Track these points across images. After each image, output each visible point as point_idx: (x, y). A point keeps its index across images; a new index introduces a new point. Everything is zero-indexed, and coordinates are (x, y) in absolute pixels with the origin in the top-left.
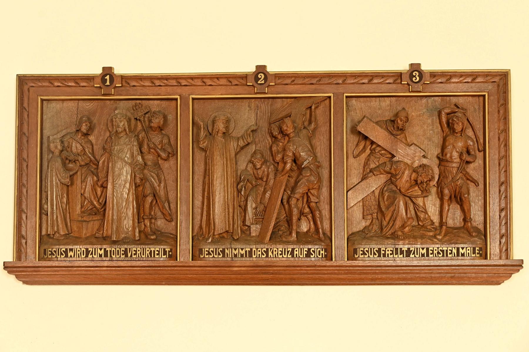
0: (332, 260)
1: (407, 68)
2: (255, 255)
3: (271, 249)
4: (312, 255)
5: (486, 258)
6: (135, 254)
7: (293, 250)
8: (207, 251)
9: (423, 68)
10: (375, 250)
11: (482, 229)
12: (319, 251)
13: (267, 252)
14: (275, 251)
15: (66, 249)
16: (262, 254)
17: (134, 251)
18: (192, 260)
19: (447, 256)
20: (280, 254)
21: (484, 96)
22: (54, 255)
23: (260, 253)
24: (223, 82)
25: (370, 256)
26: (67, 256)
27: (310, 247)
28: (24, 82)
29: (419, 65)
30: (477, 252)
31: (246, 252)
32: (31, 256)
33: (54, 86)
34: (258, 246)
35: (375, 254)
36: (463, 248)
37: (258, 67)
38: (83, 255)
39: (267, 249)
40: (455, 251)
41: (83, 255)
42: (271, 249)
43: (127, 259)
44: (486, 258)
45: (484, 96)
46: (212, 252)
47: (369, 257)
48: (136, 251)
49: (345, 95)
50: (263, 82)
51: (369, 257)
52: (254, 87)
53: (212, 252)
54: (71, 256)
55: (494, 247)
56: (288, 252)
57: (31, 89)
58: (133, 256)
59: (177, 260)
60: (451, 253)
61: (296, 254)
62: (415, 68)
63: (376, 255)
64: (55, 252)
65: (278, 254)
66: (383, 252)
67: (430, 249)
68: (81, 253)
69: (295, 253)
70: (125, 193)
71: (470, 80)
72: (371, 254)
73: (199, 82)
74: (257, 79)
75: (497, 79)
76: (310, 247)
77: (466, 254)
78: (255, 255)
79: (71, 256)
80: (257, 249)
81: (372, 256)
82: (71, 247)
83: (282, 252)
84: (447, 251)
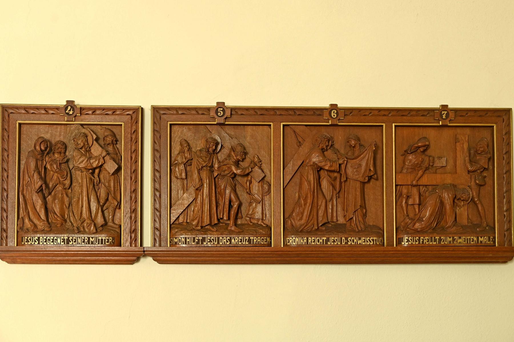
0: (121, 246)
1: (215, 104)
5: (120, 245)
7: (39, 238)
9: (76, 103)
13: (230, 240)
18: (17, 245)
19: (105, 243)
21: (171, 125)
23: (225, 241)
24: (414, 113)
28: (508, 111)
29: (224, 103)
30: (491, 240)
31: (323, 240)
33: (238, 115)
34: (223, 236)
36: (481, 237)
37: (218, 103)
40: (183, 240)
43: (198, 245)
44: (120, 245)
45: (171, 125)
49: (169, 123)
50: (443, 112)
52: (76, 116)
55: (125, 237)
56: (246, 240)
60: (108, 242)
62: (70, 103)
64: (30, 239)
66: (421, 240)
73: (252, 112)
74: (217, 112)
75: (130, 112)
77: (100, 242)
84: (105, 240)
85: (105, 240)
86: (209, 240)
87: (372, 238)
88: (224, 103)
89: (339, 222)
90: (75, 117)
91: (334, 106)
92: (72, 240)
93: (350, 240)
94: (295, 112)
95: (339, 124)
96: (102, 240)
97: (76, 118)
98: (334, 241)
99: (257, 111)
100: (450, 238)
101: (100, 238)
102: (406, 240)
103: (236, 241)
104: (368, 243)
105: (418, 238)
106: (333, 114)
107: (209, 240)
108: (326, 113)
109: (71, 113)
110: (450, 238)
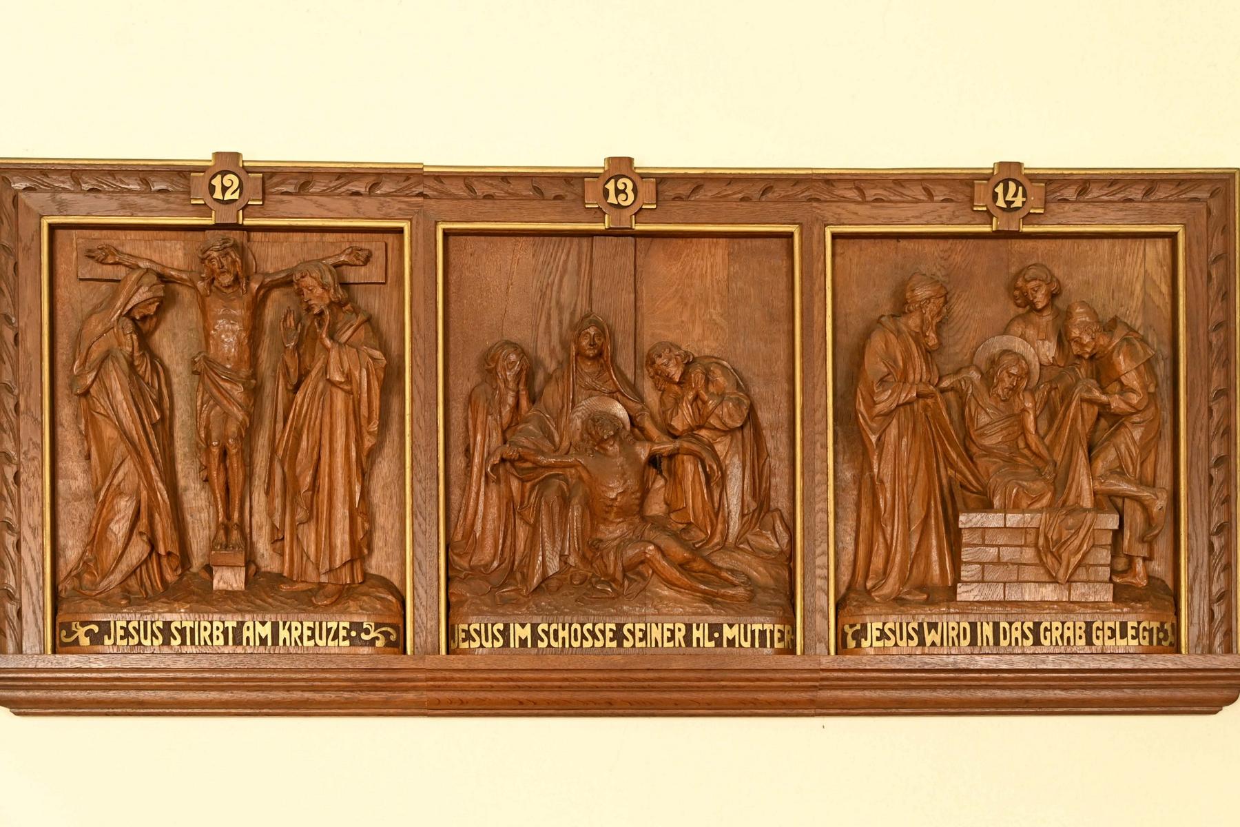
0: (1178, 651)
2: (1005, 638)
3: (285, 623)
4: (542, 640)
6: (669, 640)
8: (122, 628)
10: (910, 627)
11: (1170, 583)
12: (556, 632)
14: (205, 629)
15: (920, 625)
16: (1024, 636)
17: (309, 628)
18: (448, 652)
20: (310, 638)
22: (889, 639)
23: (1018, 634)
25: (899, 643)
26: (922, 643)
27: (168, 617)
29: (630, 160)
32: (29, 643)
35: (910, 637)
37: (612, 161)
38: (965, 638)
39: (920, 625)
41: (965, 638)
42: (285, 623)
45: (53, 228)
46: (478, 632)
47: (896, 645)
48: (673, 632)
51: (896, 645)
52: (247, 205)
53: (478, 632)
54: (933, 644)
57: (1202, 207)
58: (306, 643)
59: (405, 652)
61: (248, 638)
63: (912, 639)
65: (211, 636)
67: (1130, 624)
68: (958, 636)
69: (246, 634)
70: (422, 463)
71: (291, 189)
72: (487, 640)
73: (458, 189)
76: (168, 617)
78: (1005, 638)
79: (933, 644)
80: (1011, 624)
81: (902, 644)
82: (934, 619)
83: (313, 630)
84: (772, 632)
85: (772, 632)
86: (121, 632)
87: (600, 626)
88: (630, 160)
89: (963, 568)
90: (243, 209)
91: (621, 167)
92: (633, 634)
93: (547, 633)
94: (470, 188)
95: (1026, 229)
96: (762, 633)
97: (248, 209)
98: (883, 636)
99: (543, 185)
100: (523, 626)
101: (757, 627)
102: (121, 632)
103: (296, 634)
104: (587, 644)
105: (501, 626)
106: (232, 180)
107: (121, 632)
108: (981, 190)
109: (1018, 202)
110: (523, 626)
